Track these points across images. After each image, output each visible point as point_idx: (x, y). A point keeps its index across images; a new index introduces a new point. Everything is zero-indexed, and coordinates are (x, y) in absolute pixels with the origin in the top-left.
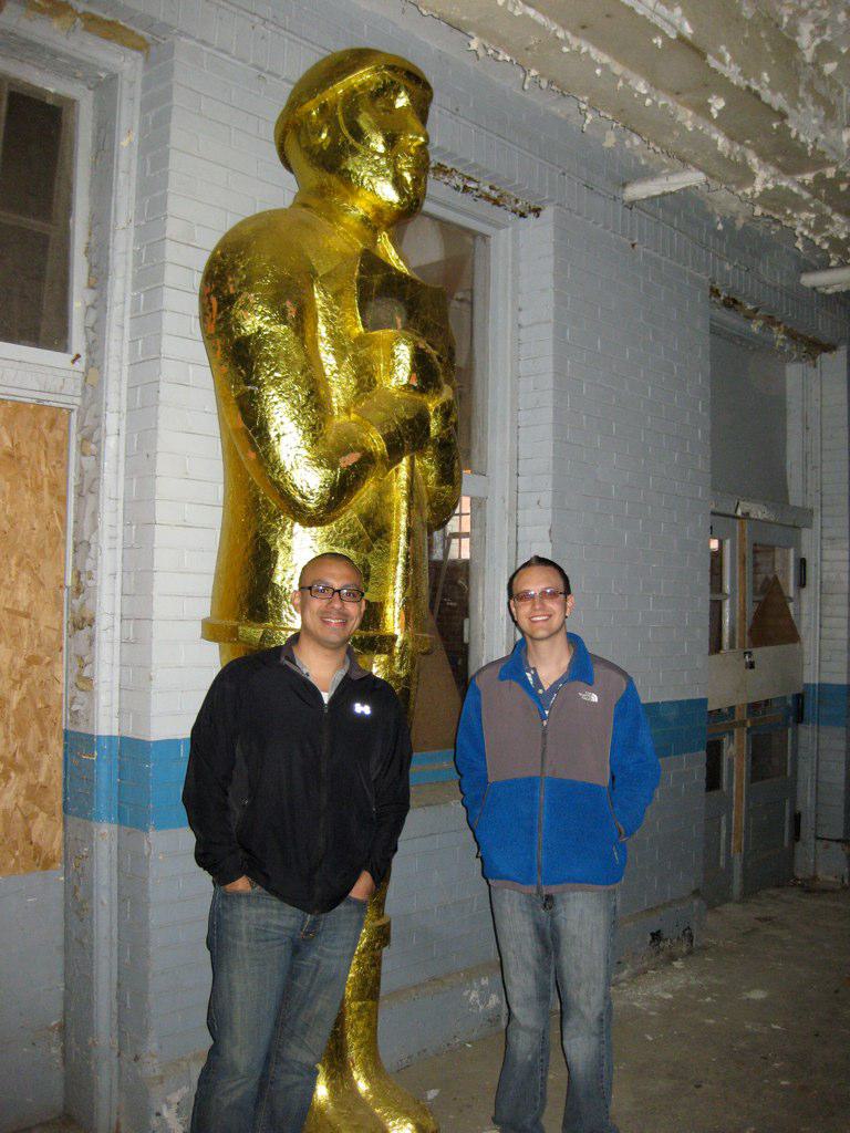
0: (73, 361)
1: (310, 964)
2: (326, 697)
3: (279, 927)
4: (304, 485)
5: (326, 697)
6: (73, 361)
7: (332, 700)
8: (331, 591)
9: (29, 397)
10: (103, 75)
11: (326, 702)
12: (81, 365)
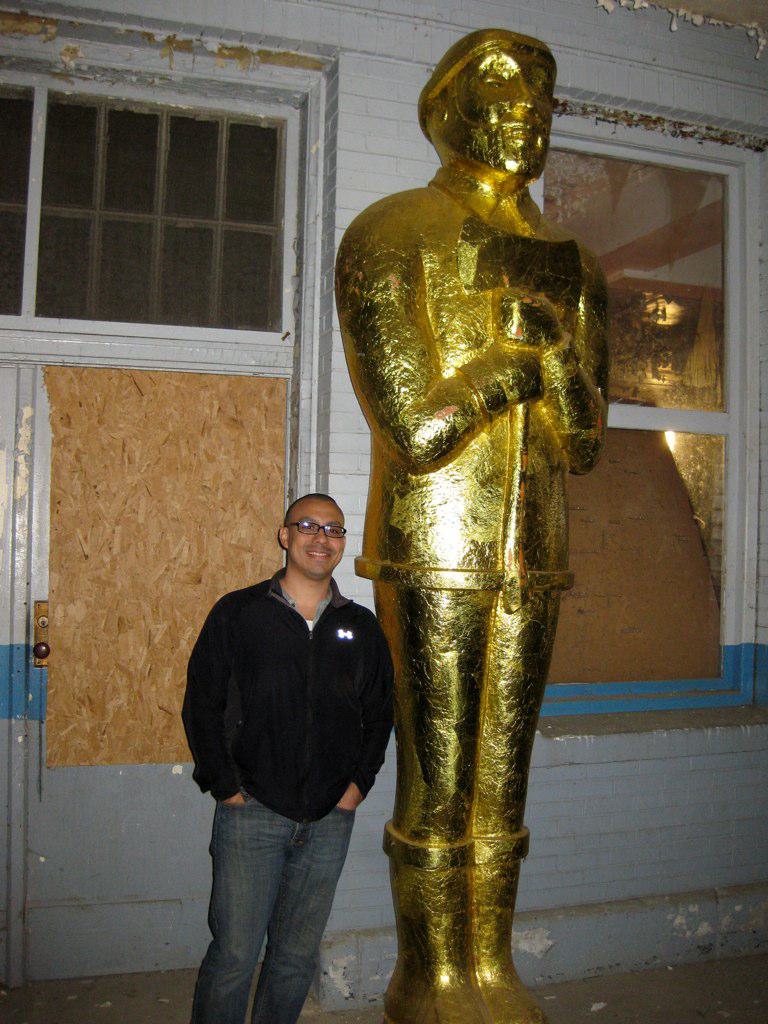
0: (284, 339)
1: (300, 867)
2: (311, 625)
3: (269, 836)
4: (431, 425)
5: (311, 625)
6: (284, 339)
7: (316, 627)
8: (316, 527)
9: (247, 371)
10: (298, 96)
11: (311, 629)
12: (291, 341)
